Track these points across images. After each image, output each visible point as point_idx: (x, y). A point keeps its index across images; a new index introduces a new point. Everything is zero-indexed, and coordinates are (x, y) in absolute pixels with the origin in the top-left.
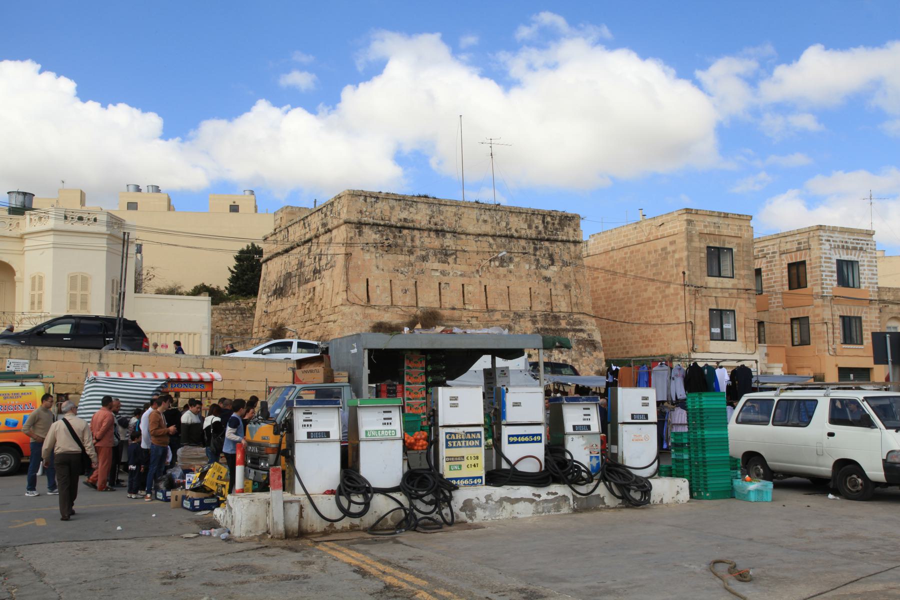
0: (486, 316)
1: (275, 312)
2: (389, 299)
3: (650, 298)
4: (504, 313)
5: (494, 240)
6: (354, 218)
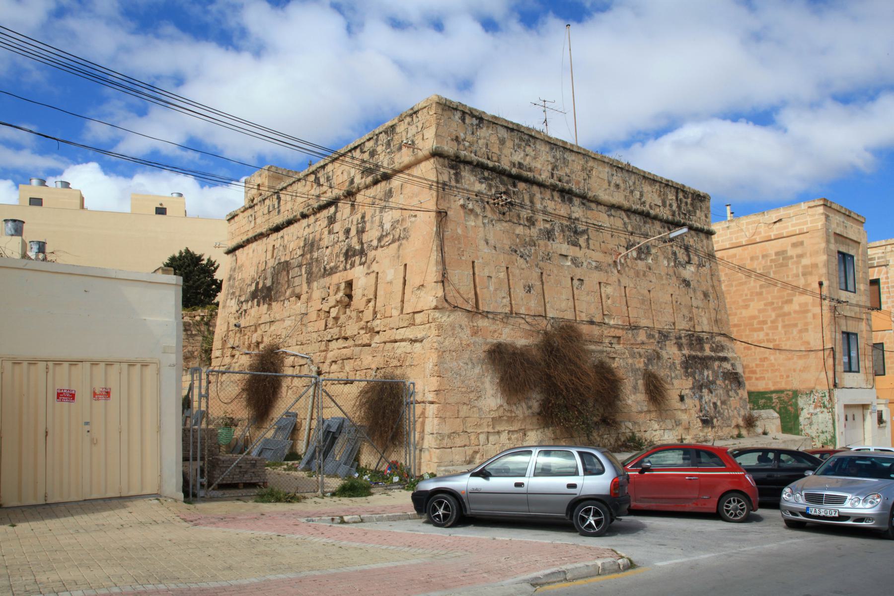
1: (256, 327)
2: (506, 301)
3: (753, 317)
5: (628, 217)
6: (449, 148)
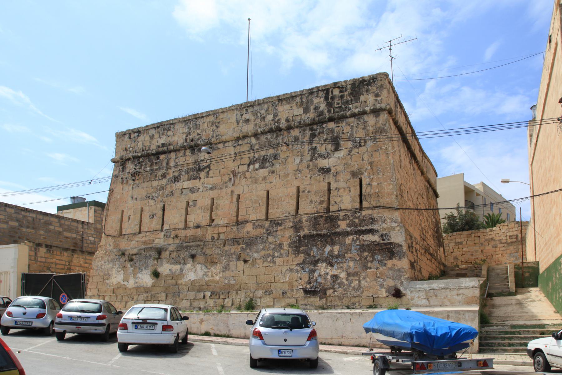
0: (235, 230)
4: (257, 224)
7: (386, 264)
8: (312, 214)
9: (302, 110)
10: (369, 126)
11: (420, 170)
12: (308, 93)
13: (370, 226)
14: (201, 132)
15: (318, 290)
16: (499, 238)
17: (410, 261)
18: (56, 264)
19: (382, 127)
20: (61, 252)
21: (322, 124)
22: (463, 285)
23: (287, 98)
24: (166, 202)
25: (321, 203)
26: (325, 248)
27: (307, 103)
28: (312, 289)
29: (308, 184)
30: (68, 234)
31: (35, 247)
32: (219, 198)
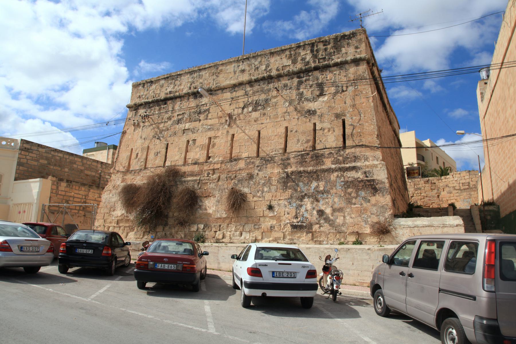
4: (248, 161)
7: (369, 200)
8: (299, 152)
9: (291, 61)
10: (350, 74)
11: (388, 120)
12: (296, 47)
13: (354, 163)
14: (204, 81)
15: (305, 224)
16: (452, 185)
17: (392, 198)
18: (74, 197)
19: (362, 74)
20: (79, 187)
21: (308, 73)
22: (447, 223)
23: (278, 51)
24: (169, 141)
25: (308, 141)
26: (311, 184)
27: (294, 55)
28: (299, 224)
29: (295, 124)
30: (89, 173)
31: (57, 181)
32: (215, 137)
